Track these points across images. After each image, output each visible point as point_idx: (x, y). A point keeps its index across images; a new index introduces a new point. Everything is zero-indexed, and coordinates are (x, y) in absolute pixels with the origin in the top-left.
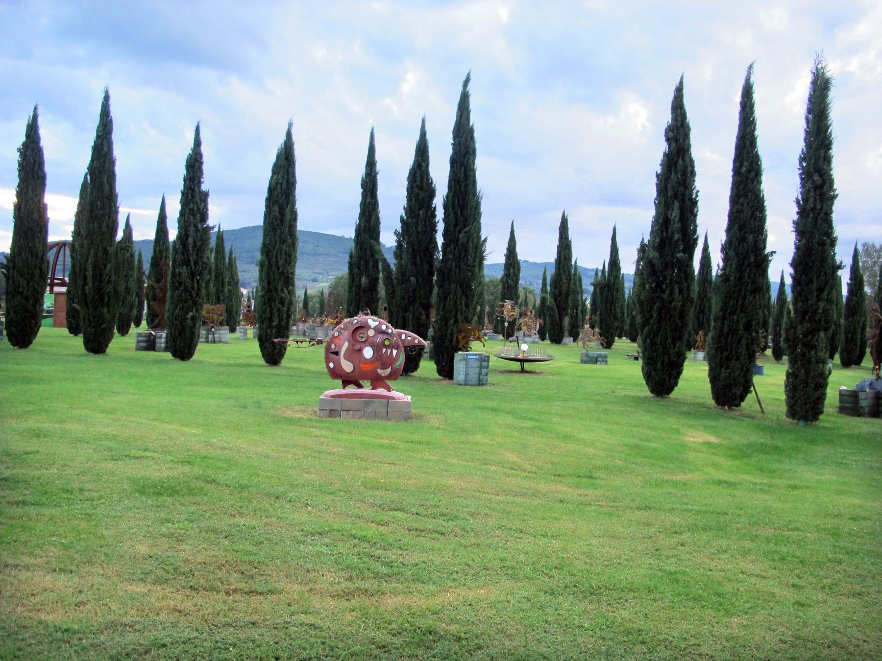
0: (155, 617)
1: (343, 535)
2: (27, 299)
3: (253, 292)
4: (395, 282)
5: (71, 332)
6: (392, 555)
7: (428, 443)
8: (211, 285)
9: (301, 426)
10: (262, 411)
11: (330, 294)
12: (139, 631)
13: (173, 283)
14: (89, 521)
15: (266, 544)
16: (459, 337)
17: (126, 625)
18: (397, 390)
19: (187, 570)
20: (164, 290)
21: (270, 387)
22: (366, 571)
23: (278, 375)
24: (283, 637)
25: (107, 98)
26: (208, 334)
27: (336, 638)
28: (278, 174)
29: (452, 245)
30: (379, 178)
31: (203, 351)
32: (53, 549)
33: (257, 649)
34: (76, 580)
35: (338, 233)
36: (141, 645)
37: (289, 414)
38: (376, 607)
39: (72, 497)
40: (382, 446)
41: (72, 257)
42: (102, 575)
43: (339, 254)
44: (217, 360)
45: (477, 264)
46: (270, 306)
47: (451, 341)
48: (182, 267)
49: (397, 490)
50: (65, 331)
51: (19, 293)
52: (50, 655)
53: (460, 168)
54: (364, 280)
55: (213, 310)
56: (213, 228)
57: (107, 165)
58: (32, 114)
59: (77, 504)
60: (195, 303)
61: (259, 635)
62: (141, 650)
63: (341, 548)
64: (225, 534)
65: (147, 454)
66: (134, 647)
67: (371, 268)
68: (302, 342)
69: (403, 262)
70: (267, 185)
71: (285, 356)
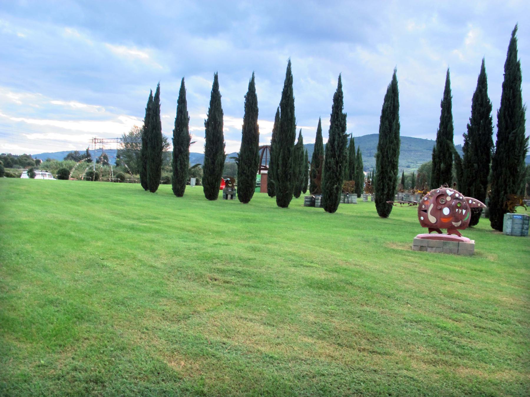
0: (318, 358)
1: (431, 324)
2: (248, 176)
3: (370, 174)
4: (463, 167)
5: (269, 195)
6: (463, 341)
7: (486, 272)
8: (347, 170)
9: (402, 255)
10: (378, 245)
11: (419, 175)
12: (310, 364)
13: (326, 168)
14: (282, 299)
15: (382, 324)
16: (508, 203)
17: (302, 360)
18: (464, 236)
19: (336, 333)
20: (320, 172)
21: (382, 231)
22: (446, 349)
23: (387, 223)
24: (394, 382)
25: (289, 64)
26: (345, 198)
27: (427, 389)
28: (388, 101)
29: (504, 142)
30: (453, 100)
31: (342, 208)
32: (264, 312)
33: (378, 387)
34: (276, 330)
35: (423, 137)
36: (311, 372)
37: (394, 247)
38: (453, 374)
39: (273, 285)
40: (455, 271)
41: (271, 154)
42: (290, 330)
43: (424, 151)
44: (351, 214)
45: (521, 154)
46: (383, 182)
47: (502, 205)
48: (331, 158)
49: (466, 300)
50: (266, 195)
51: (244, 173)
52: (264, 369)
53: (510, 91)
54: (442, 165)
55: (348, 184)
56: (349, 135)
57: (290, 102)
58: (251, 77)
59: (276, 289)
60: (338, 180)
61: (378, 378)
62: (311, 375)
63: (430, 333)
64: (358, 315)
65: (312, 265)
66: (307, 373)
67: (447, 158)
68: (403, 203)
69: (469, 154)
70: (381, 108)
71: (391, 212)
